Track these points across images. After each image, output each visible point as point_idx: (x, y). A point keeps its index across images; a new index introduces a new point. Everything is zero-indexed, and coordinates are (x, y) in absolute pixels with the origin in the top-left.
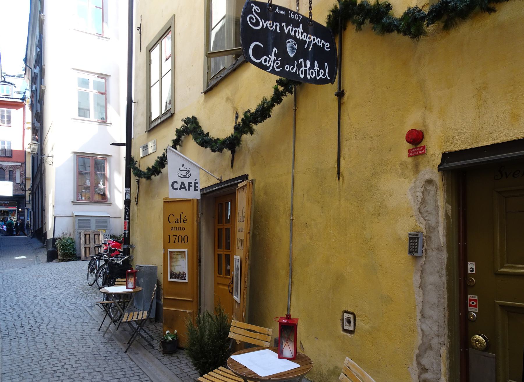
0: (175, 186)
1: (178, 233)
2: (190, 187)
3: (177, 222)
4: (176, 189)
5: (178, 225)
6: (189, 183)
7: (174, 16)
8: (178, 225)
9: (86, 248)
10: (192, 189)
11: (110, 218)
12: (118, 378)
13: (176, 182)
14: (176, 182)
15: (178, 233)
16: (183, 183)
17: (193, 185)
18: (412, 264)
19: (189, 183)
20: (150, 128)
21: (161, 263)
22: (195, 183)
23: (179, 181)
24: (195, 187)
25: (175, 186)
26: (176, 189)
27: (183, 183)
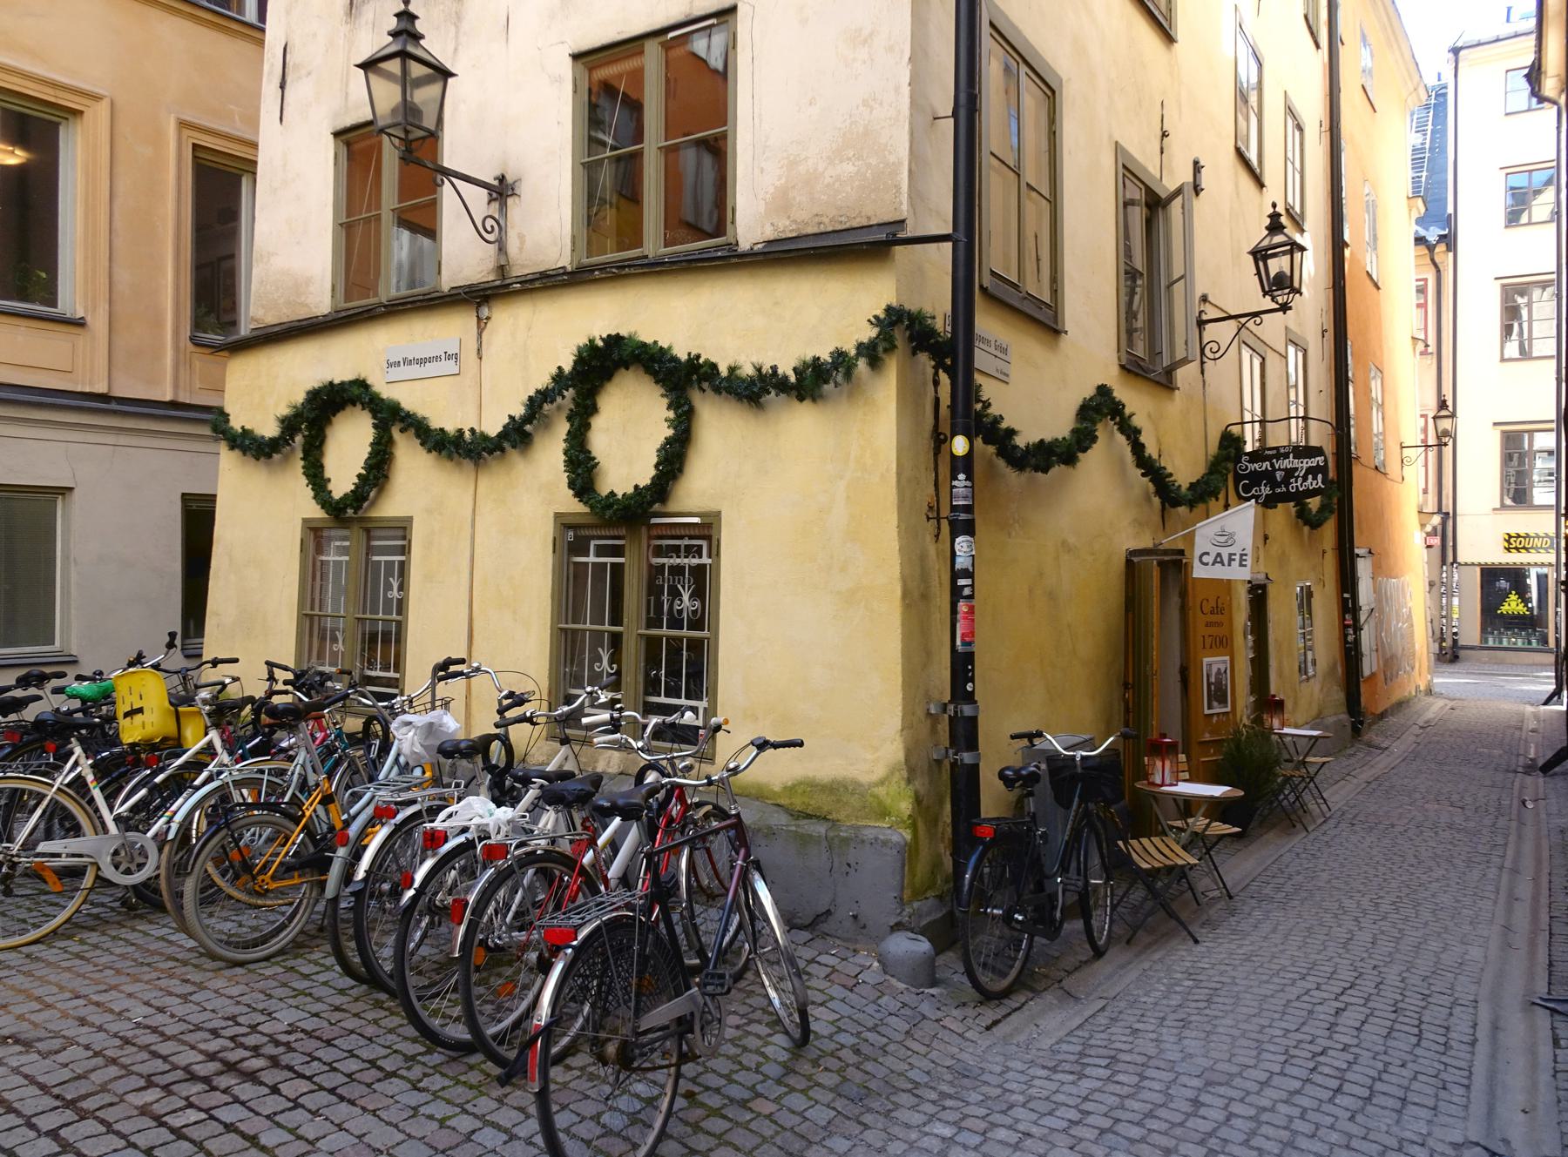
0: (1205, 559)
1: (1213, 631)
2: (1231, 560)
3: (1212, 613)
4: (1207, 564)
5: (1214, 618)
6: (1230, 555)
7: (1168, 37)
8: (1214, 618)
9: (652, 644)
10: (1235, 564)
11: (378, 112)
12: (7, 1126)
13: (1208, 554)
14: (1208, 554)
15: (1213, 631)
16: (1219, 555)
17: (1237, 557)
18: (1234, 932)
19: (1230, 555)
20: (992, 25)
21: (909, 235)
22: (1242, 555)
23: (1214, 551)
24: (1241, 560)
25: (1205, 559)
26: (1207, 564)
27: (1219, 555)
